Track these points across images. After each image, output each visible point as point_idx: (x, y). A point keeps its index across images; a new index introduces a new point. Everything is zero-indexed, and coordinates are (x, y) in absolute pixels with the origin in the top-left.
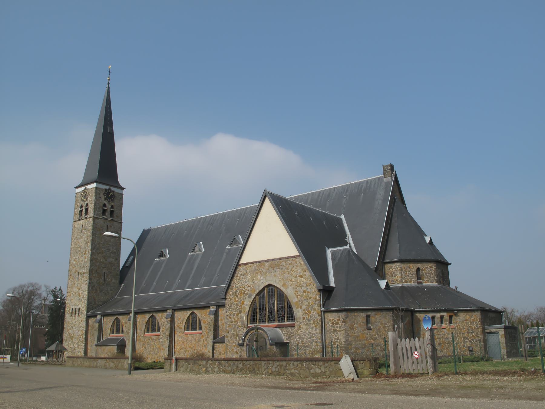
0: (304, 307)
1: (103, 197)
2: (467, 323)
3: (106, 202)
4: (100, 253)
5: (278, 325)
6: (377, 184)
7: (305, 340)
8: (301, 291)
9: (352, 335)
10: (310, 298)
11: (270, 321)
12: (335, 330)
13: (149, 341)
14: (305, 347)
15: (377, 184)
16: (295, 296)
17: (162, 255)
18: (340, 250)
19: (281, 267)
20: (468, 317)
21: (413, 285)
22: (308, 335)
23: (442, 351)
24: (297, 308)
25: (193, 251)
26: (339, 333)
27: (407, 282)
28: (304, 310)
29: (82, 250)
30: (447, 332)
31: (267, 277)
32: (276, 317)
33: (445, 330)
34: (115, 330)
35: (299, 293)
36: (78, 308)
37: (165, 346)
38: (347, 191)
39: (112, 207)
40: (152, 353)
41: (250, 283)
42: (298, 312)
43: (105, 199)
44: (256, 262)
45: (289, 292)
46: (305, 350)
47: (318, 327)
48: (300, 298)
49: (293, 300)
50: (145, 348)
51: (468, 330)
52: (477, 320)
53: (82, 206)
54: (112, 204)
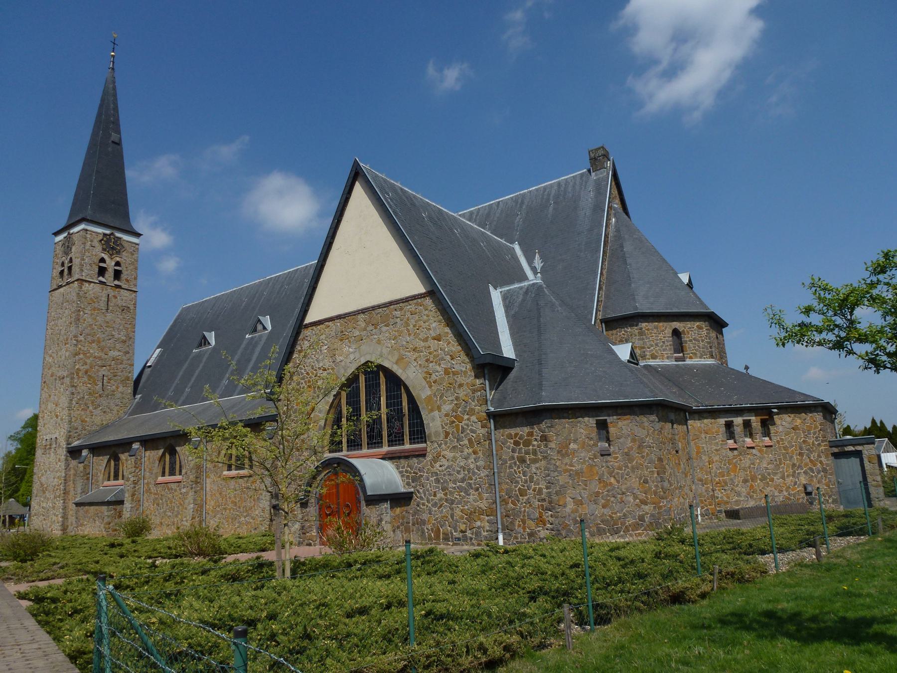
0: (447, 408)
1: (99, 247)
2: (20, 500)
3: (106, 257)
4: (93, 342)
5: (388, 453)
6: (578, 183)
7: (451, 485)
8: (438, 370)
9: (566, 471)
10: (461, 385)
11: (371, 445)
12: (522, 460)
13: (163, 493)
14: (452, 502)
15: (578, 183)
16: (424, 383)
17: (204, 341)
18: (521, 288)
19: (392, 321)
20: (798, 422)
21: (667, 362)
22: (458, 472)
23: (751, 497)
24: (432, 410)
25: (255, 330)
26: (533, 467)
27: (654, 357)
28: (447, 415)
29: (61, 338)
30: (759, 454)
31: (363, 347)
32: (385, 433)
33: (754, 451)
34: (112, 474)
35: (434, 377)
36: (54, 437)
37: (187, 501)
38: (522, 203)
39: (118, 264)
40: (169, 514)
41: (327, 363)
42: (433, 420)
43: (104, 250)
44: (339, 317)
45: (411, 375)
46: (452, 509)
47: (480, 454)
48: (435, 387)
49: (422, 392)
50: (158, 505)
51: (801, 448)
52: (816, 427)
53: (63, 264)
54: (118, 259)
